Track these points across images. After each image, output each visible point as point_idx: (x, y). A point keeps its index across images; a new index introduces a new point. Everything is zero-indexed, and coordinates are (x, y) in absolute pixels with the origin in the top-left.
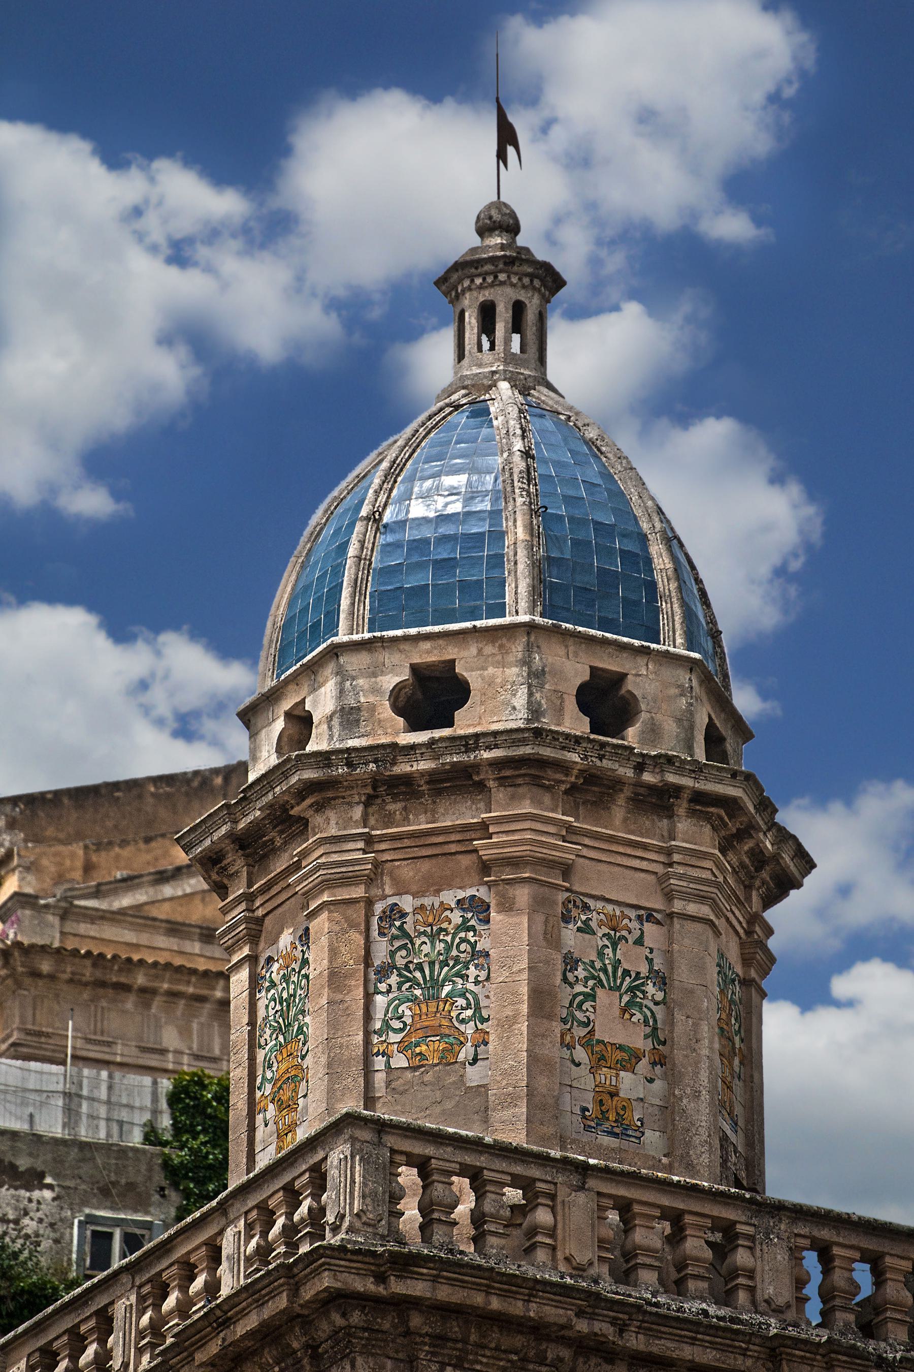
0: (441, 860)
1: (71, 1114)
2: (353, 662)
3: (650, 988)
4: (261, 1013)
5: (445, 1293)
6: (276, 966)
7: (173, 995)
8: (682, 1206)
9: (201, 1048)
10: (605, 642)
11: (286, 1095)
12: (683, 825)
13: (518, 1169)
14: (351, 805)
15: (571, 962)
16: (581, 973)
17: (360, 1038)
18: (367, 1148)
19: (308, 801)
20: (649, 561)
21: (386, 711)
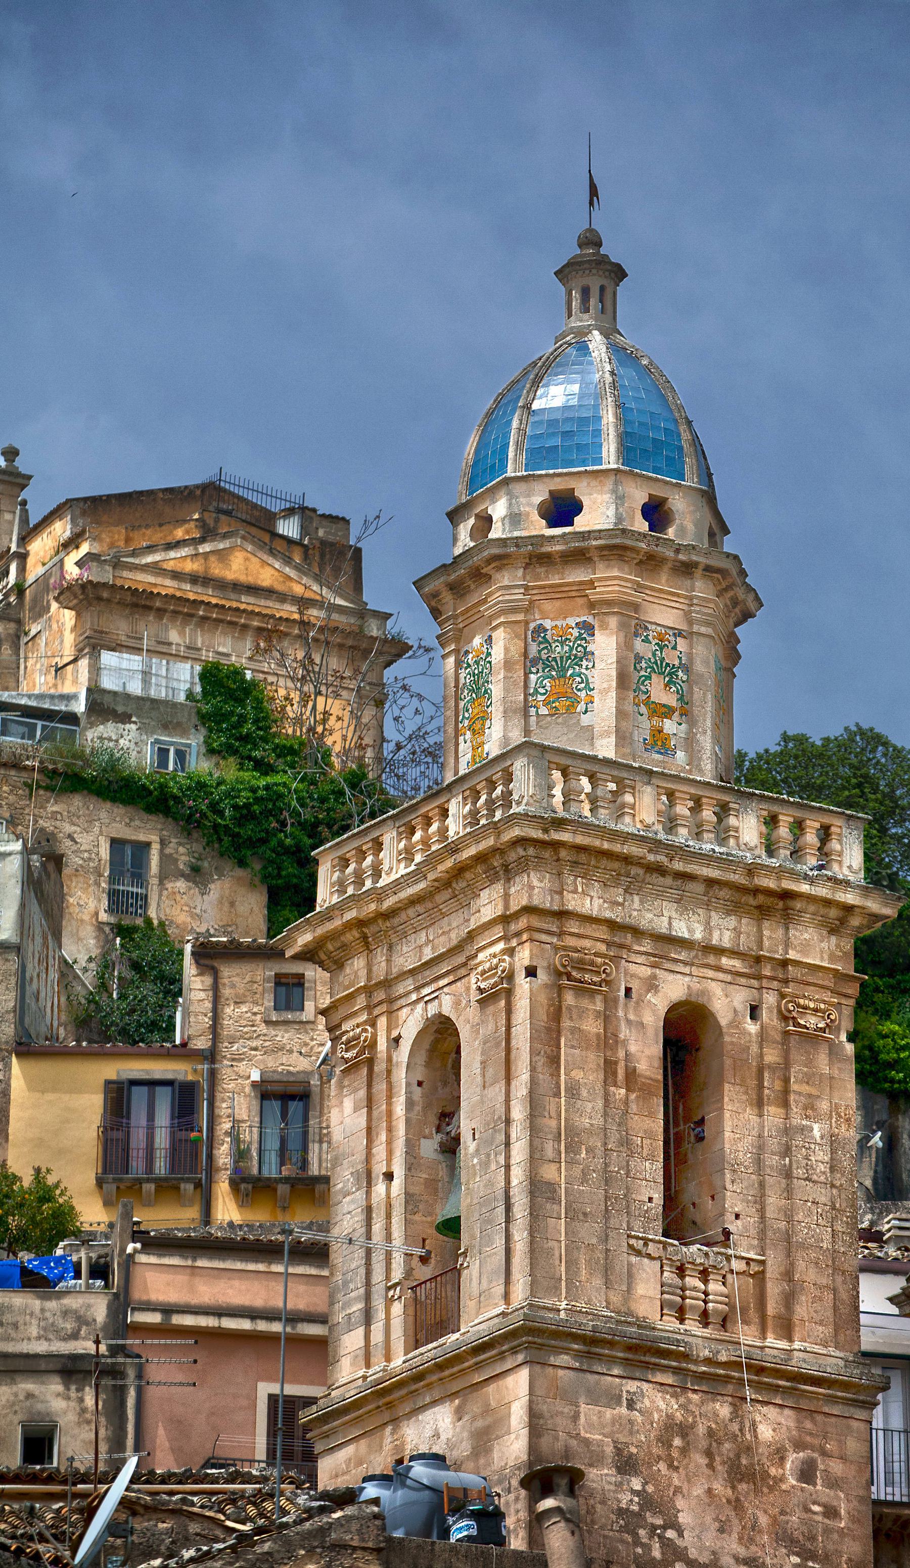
0: (567, 600)
1: (146, 682)
2: (518, 488)
3: (680, 674)
4: (462, 681)
5: (580, 840)
6: (470, 656)
7: (175, 612)
8: (701, 793)
9: (190, 643)
10: (657, 480)
11: (477, 726)
12: (699, 584)
13: (615, 773)
14: (516, 568)
15: (638, 658)
16: (644, 665)
17: (522, 697)
18: (537, 760)
19: (493, 565)
20: (679, 435)
21: (535, 516)
